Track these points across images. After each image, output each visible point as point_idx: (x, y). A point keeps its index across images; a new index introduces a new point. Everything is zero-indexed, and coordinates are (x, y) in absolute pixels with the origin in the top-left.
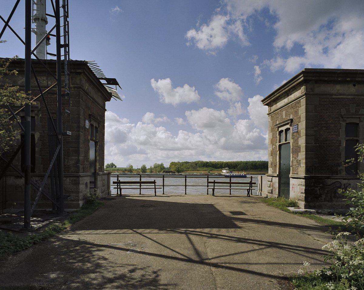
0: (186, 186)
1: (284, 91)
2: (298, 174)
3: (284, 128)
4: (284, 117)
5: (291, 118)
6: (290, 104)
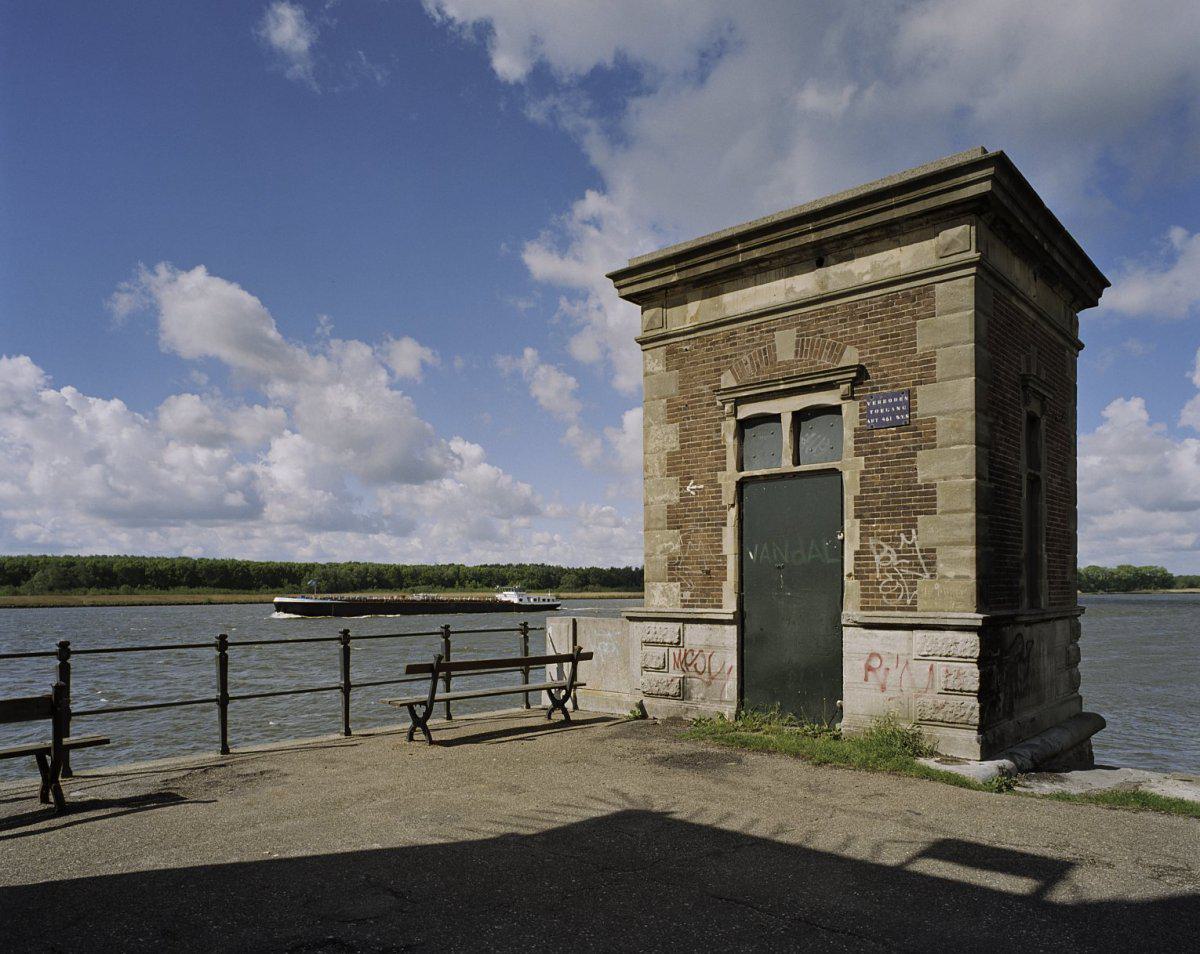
1: (813, 237)
2: (915, 610)
6: (837, 302)
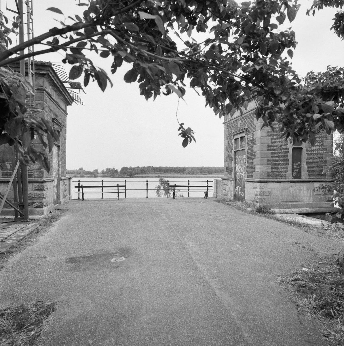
0: (147, 190)
3: (239, 136)
4: (239, 126)
5: (246, 127)
